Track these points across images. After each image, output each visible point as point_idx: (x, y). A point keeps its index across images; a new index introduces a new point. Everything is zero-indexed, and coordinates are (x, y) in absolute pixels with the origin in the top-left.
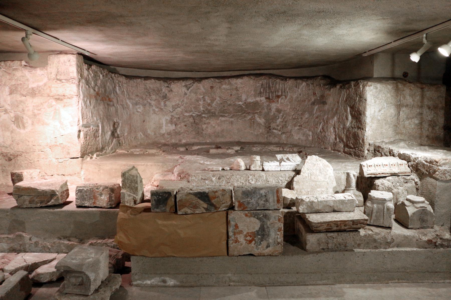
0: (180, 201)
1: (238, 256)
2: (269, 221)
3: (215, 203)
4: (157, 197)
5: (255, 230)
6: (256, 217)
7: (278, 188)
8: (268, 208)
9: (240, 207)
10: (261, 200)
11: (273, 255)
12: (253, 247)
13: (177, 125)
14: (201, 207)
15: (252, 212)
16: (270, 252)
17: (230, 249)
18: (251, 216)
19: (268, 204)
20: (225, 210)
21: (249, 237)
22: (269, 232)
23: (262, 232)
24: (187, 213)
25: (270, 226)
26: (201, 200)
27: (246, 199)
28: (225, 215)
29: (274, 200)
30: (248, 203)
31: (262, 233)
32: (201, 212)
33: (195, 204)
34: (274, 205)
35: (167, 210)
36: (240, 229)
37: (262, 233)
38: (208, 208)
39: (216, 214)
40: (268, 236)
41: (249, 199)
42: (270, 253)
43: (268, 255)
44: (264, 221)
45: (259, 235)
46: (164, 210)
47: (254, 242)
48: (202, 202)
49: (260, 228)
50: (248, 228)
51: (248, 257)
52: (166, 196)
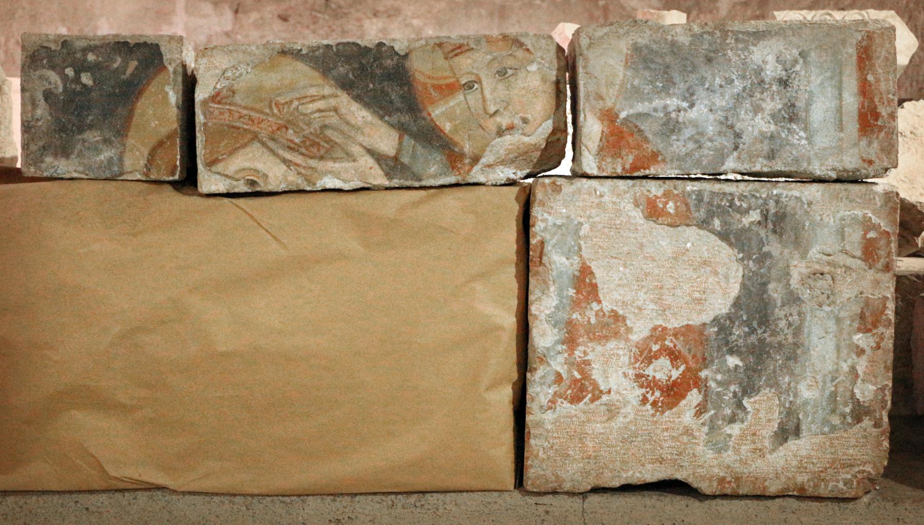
0: (216, 98)
1: (584, 495)
2: (804, 256)
3: (447, 127)
4: (65, 78)
5: (707, 318)
6: (717, 223)
7: (870, 36)
8: (796, 160)
9: (617, 155)
10: (757, 109)
11: (823, 491)
12: (688, 432)
13: (246, 12)
14: (356, 150)
15: (690, 187)
16: (801, 468)
17: (534, 443)
18: (681, 220)
19: (798, 137)
20: (511, 183)
21: (664, 362)
22: (798, 331)
23: (753, 331)
24: (262, 187)
25: (806, 294)
26: (357, 98)
27: (657, 103)
28: (515, 208)
29: (840, 110)
30: (671, 127)
31: (753, 339)
32: (358, 184)
33: (316, 126)
34: (840, 150)
35: (128, 163)
36: (607, 306)
37: (753, 339)
38: (405, 160)
39: (452, 201)
40: (792, 357)
41: (673, 102)
42: (801, 478)
43: (781, 495)
44: (764, 257)
45: (731, 352)
46: (110, 161)
47: (694, 397)
48: (359, 114)
49: (737, 304)
50: (658, 301)
51: (651, 501)
52: (129, 71)
